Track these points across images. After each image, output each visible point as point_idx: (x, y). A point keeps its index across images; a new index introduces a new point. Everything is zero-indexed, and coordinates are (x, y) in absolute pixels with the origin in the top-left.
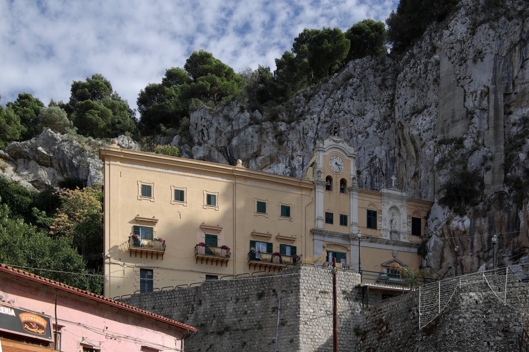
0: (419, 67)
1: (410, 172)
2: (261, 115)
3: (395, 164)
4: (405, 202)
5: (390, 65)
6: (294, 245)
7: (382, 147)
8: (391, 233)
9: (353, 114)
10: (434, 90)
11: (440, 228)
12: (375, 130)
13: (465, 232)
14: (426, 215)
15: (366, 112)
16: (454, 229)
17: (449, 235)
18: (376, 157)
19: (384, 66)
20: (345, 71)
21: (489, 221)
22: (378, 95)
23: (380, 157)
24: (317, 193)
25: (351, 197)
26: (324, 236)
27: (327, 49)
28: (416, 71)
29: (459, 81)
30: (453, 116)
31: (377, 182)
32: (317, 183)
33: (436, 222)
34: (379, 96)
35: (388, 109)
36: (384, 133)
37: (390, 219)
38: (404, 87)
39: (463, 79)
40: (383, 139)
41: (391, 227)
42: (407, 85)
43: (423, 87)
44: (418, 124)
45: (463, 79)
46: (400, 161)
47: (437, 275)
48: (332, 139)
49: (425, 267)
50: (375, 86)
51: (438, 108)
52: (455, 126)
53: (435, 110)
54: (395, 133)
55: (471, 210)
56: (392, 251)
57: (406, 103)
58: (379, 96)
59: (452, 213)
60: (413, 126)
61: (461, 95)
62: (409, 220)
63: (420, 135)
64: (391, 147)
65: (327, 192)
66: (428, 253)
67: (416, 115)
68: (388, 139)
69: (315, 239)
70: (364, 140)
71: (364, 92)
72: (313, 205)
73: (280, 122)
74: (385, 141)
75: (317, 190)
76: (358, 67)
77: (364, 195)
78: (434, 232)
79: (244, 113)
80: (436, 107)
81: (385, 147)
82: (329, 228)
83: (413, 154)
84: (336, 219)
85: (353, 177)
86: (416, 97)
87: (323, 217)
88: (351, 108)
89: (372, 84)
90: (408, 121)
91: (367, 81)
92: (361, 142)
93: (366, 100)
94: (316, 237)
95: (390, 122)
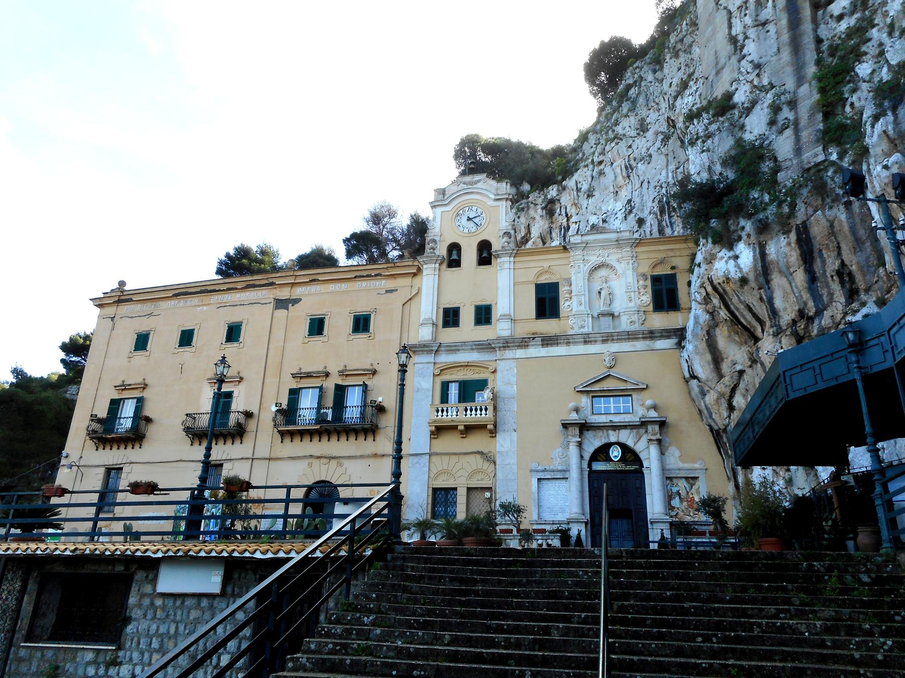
13: (744, 281)
16: (721, 281)
21: (799, 241)
30: (717, 64)
31: (667, 227)
55: (748, 226)
59: (710, 245)
82: (450, 335)
84: (467, 316)
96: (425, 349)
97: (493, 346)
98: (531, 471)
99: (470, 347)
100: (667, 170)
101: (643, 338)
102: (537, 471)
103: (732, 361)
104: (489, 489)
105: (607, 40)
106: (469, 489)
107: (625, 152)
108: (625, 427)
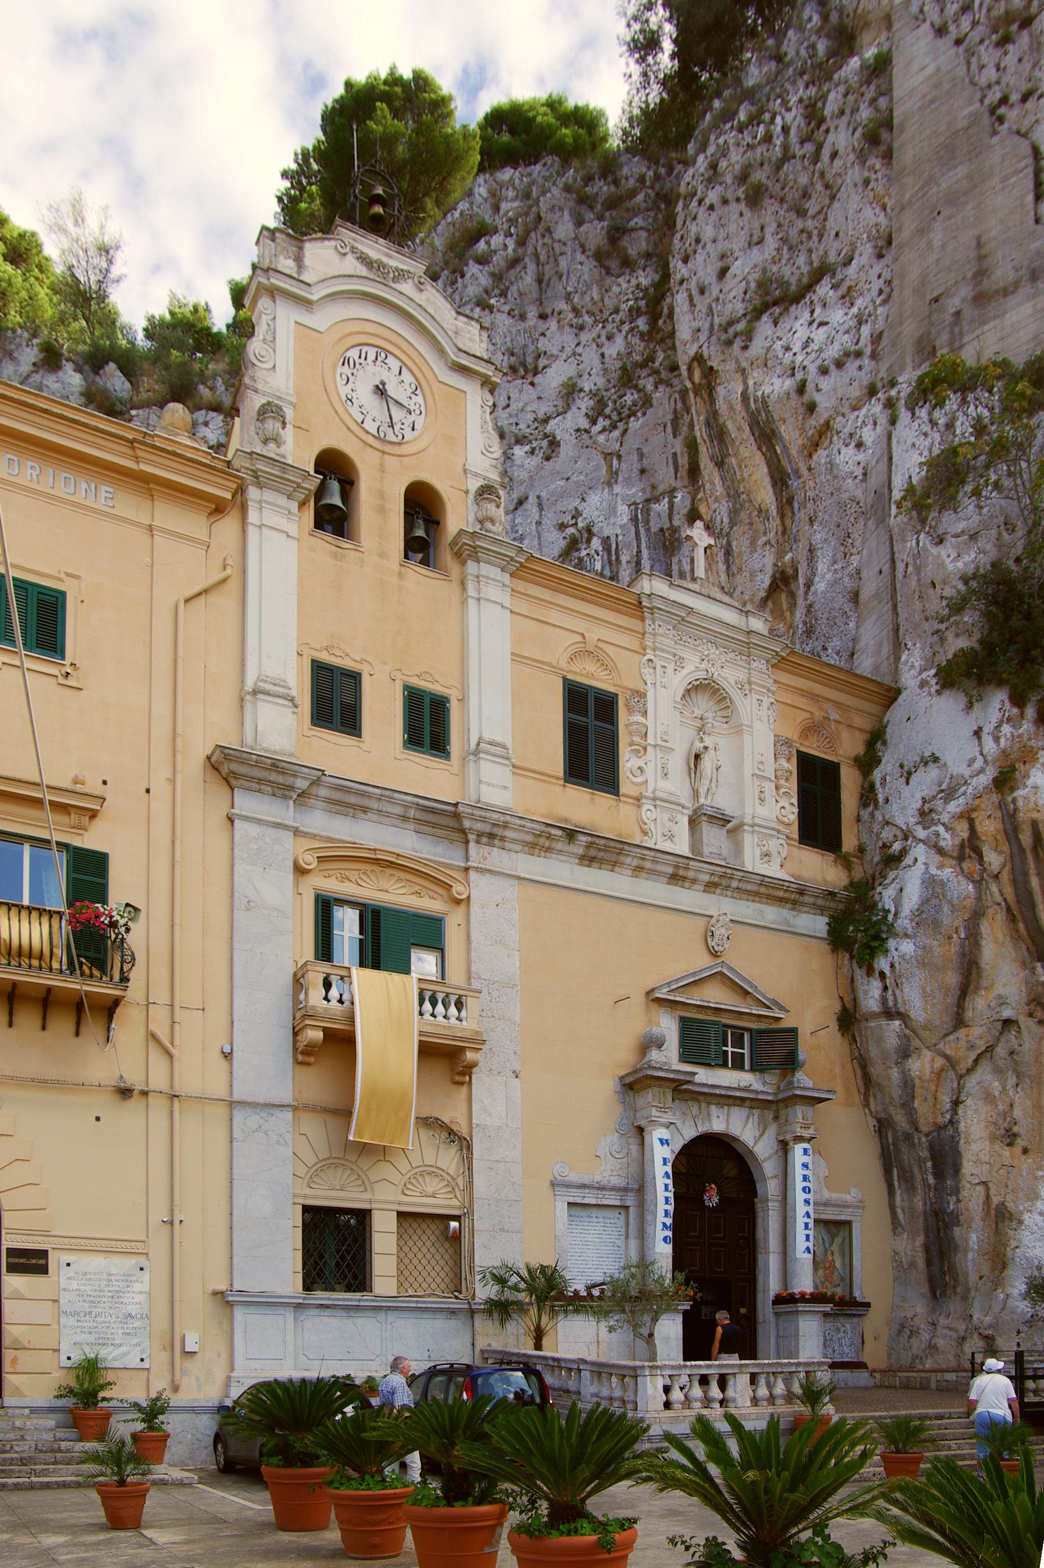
0: (778, 120)
1: (753, 575)
2: (128, 385)
3: (675, 560)
4: (759, 665)
5: (642, 180)
6: (91, 840)
7: (617, 489)
8: (693, 822)
10: (866, 182)
11: (954, 807)
12: (584, 423)
14: (860, 749)
15: (542, 362)
17: (1006, 848)
18: (589, 531)
19: (616, 183)
22: (595, 293)
23: (606, 532)
24: (252, 533)
25: (471, 591)
27: (389, 140)
28: (768, 139)
29: (1002, 110)
30: (980, 274)
32: (255, 473)
33: (926, 781)
34: (596, 297)
35: (635, 341)
36: (625, 431)
37: (686, 746)
38: (711, 208)
39: (1025, 98)
40: (619, 457)
41: (696, 794)
42: (729, 196)
43: (806, 195)
44: (788, 349)
45: (1025, 98)
47: (939, 1062)
48: (353, 250)
49: (874, 1015)
50: (579, 257)
51: (888, 259)
52: (995, 318)
53: (876, 270)
54: (669, 429)
56: (701, 922)
57: (723, 273)
58: (596, 297)
59: (1027, 727)
61: (1017, 172)
62: (786, 765)
63: (801, 389)
64: (654, 487)
65: (324, 543)
66: (891, 944)
67: (777, 310)
68: (641, 456)
69: (246, 818)
70: (539, 468)
71: (535, 285)
72: (225, 601)
73: (203, 412)
74: (629, 466)
75: (253, 516)
76: (511, 194)
77: (546, 595)
78: (921, 833)
79: (60, 374)
80: (880, 256)
81: (635, 491)
83: (766, 495)
85: (481, 482)
86: (771, 243)
89: (568, 249)
90: (738, 343)
91: (547, 240)
92: (523, 475)
93: (543, 317)
94: (246, 803)
95: (649, 387)
96: (273, 776)
99: (398, 810)
103: (1000, 997)
108: (741, 1101)
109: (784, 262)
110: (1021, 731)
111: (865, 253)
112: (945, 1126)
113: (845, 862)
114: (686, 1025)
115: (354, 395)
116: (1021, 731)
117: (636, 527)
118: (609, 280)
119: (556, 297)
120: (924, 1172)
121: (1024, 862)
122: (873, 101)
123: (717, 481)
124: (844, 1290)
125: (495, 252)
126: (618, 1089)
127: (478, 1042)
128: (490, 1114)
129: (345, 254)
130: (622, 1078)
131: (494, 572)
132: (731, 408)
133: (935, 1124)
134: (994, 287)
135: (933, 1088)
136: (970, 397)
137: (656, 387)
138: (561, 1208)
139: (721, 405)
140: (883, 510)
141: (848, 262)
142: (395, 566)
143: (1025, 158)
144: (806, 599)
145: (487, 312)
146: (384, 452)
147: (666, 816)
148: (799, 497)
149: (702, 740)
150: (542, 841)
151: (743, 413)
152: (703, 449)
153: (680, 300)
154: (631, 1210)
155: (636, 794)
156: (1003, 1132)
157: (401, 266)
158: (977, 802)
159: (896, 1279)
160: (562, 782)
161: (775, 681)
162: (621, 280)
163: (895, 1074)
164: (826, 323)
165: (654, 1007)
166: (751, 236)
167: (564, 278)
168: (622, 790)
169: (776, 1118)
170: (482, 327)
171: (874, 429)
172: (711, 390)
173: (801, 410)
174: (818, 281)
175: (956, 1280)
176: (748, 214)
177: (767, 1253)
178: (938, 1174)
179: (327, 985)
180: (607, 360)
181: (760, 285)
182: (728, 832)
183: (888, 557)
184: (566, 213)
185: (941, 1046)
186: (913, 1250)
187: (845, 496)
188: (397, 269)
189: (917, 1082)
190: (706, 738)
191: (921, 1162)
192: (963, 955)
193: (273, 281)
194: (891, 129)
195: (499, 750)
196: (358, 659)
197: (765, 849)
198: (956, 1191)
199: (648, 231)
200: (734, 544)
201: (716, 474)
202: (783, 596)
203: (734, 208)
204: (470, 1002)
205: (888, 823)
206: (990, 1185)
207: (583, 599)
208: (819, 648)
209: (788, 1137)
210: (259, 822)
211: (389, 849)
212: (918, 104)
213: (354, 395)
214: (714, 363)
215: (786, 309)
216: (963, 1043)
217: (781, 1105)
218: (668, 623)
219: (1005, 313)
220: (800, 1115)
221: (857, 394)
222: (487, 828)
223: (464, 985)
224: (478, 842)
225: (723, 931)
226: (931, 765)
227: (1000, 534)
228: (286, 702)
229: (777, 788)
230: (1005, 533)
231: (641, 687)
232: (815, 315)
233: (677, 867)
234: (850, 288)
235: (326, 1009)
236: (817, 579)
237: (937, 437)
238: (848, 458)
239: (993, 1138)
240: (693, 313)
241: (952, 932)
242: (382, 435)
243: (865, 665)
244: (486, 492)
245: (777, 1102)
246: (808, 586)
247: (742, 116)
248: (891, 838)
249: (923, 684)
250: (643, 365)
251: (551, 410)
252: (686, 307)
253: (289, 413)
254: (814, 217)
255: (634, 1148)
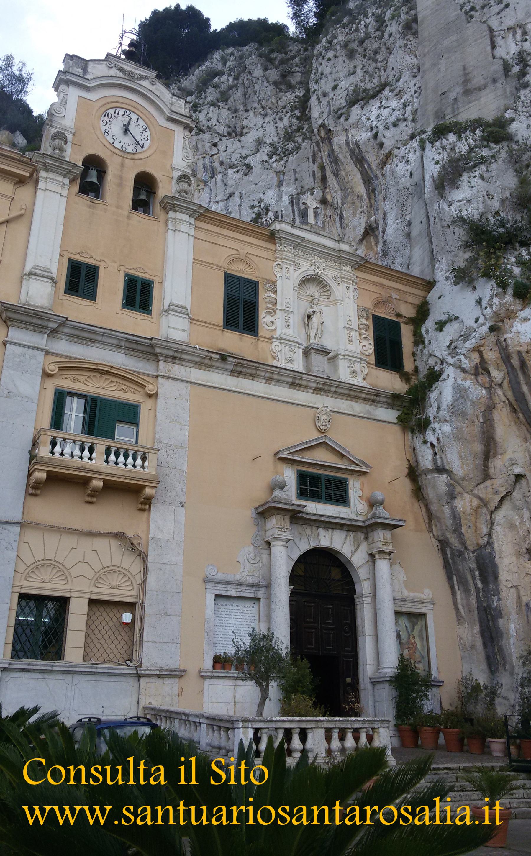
0: (363, 23)
1: (354, 228)
8: (307, 353)
9: (218, 134)
11: (469, 344)
12: (266, 158)
15: (245, 131)
16: (524, 349)
17: (504, 368)
20: (204, 67)
25: (170, 226)
26: (53, 333)
28: (357, 30)
29: (473, 13)
30: (466, 81)
32: (45, 165)
35: (294, 120)
36: (287, 161)
38: (329, 59)
39: (482, 8)
41: (308, 337)
42: (338, 54)
43: (376, 52)
44: (369, 119)
45: (482, 8)
46: (325, 215)
47: (476, 502)
48: (116, 66)
49: (430, 471)
50: (266, 84)
51: (419, 77)
52: (475, 100)
57: (335, 88)
60: (357, 125)
61: (481, 37)
63: (376, 136)
65: (83, 201)
67: (362, 102)
68: (295, 172)
78: (450, 360)
80: (415, 77)
83: (361, 189)
85: (179, 174)
86: (360, 73)
87: (54, 270)
88: (214, 121)
96: (34, 321)
97: (158, 350)
98: (206, 581)
100: (280, 192)
101: (365, 399)
102: (216, 582)
103: (511, 459)
104: (130, 606)
105: (161, 9)
106: (93, 602)
107: (208, 149)
109: (366, 81)
110: (505, 301)
111: (407, 76)
112: (485, 546)
113: (405, 377)
114: (302, 478)
115: (110, 130)
116: (505, 301)
117: (292, 206)
118: (281, 94)
119: (253, 102)
120: (474, 578)
121: (517, 376)
122: (407, 13)
123: (335, 182)
124: (424, 666)
125: (223, 83)
126: (254, 515)
127: (155, 481)
128: (162, 531)
129: (111, 68)
130: (256, 508)
131: (185, 217)
132: (340, 147)
133: (478, 544)
134: (474, 87)
135: (473, 519)
136: (463, 135)
137: (304, 141)
138: (210, 598)
139: (335, 147)
140: (421, 192)
141: (398, 80)
142: (126, 213)
143: (485, 32)
144: (383, 238)
145: (217, 108)
146: (124, 157)
147: (287, 349)
148: (378, 188)
149: (312, 307)
150: (206, 361)
151: (347, 150)
152: (327, 168)
153: (313, 100)
154: (262, 601)
155: (269, 336)
156: (525, 550)
157: (142, 74)
158: (482, 341)
159: (462, 658)
160: (222, 328)
161: (357, 277)
162: (287, 94)
163: (447, 509)
164: (388, 107)
165: (280, 465)
166: (349, 71)
167: (257, 94)
168: (259, 335)
169: (366, 538)
170: (186, 102)
171: (415, 153)
172: (330, 140)
173: (376, 147)
174: (383, 89)
175: (504, 659)
176: (347, 62)
177: (364, 635)
178: (484, 580)
179: (54, 444)
180: (279, 129)
181: (354, 91)
182: (329, 359)
183: (425, 214)
184: (259, 66)
185: (475, 491)
186: (473, 636)
187: (401, 186)
188: (140, 75)
189: (462, 515)
190: (315, 306)
191: (471, 571)
192: (483, 433)
193: (67, 77)
194: (417, 23)
195: (181, 310)
196: (98, 259)
197: (352, 369)
198: (497, 592)
199: (301, 73)
200: (344, 213)
201: (334, 179)
202: (372, 238)
203: (341, 59)
204: (150, 456)
205: (431, 355)
206: (519, 587)
207: (239, 233)
208: (390, 263)
209: (375, 551)
210: (23, 346)
211: (107, 364)
212: (430, 12)
213: (110, 130)
214: (331, 128)
215: (368, 102)
216: (490, 490)
217: (369, 529)
218: (290, 245)
219: (480, 98)
220: (382, 536)
221: (406, 138)
222: (171, 353)
223: (149, 445)
224: (165, 361)
225: (325, 417)
226: (454, 322)
227: (484, 200)
228: (48, 280)
229: (360, 335)
230: (487, 200)
231: (273, 279)
232: (382, 104)
233: (294, 378)
234: (400, 91)
235: (50, 459)
236: (388, 227)
237: (446, 155)
238: (401, 168)
239: (518, 554)
240: (320, 105)
241: (475, 419)
242: (124, 149)
243: (416, 271)
244: (183, 178)
245: (366, 527)
246: (384, 231)
247: (345, 21)
248: (434, 364)
249: (447, 278)
250: (298, 130)
251: (248, 152)
252: (316, 103)
253: (69, 137)
254: (381, 62)
255: (265, 557)
